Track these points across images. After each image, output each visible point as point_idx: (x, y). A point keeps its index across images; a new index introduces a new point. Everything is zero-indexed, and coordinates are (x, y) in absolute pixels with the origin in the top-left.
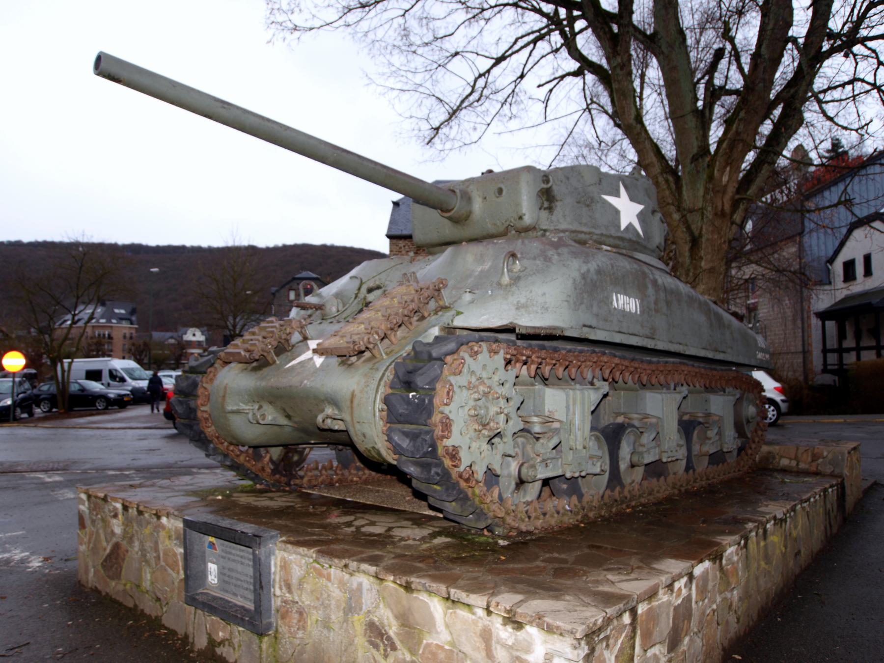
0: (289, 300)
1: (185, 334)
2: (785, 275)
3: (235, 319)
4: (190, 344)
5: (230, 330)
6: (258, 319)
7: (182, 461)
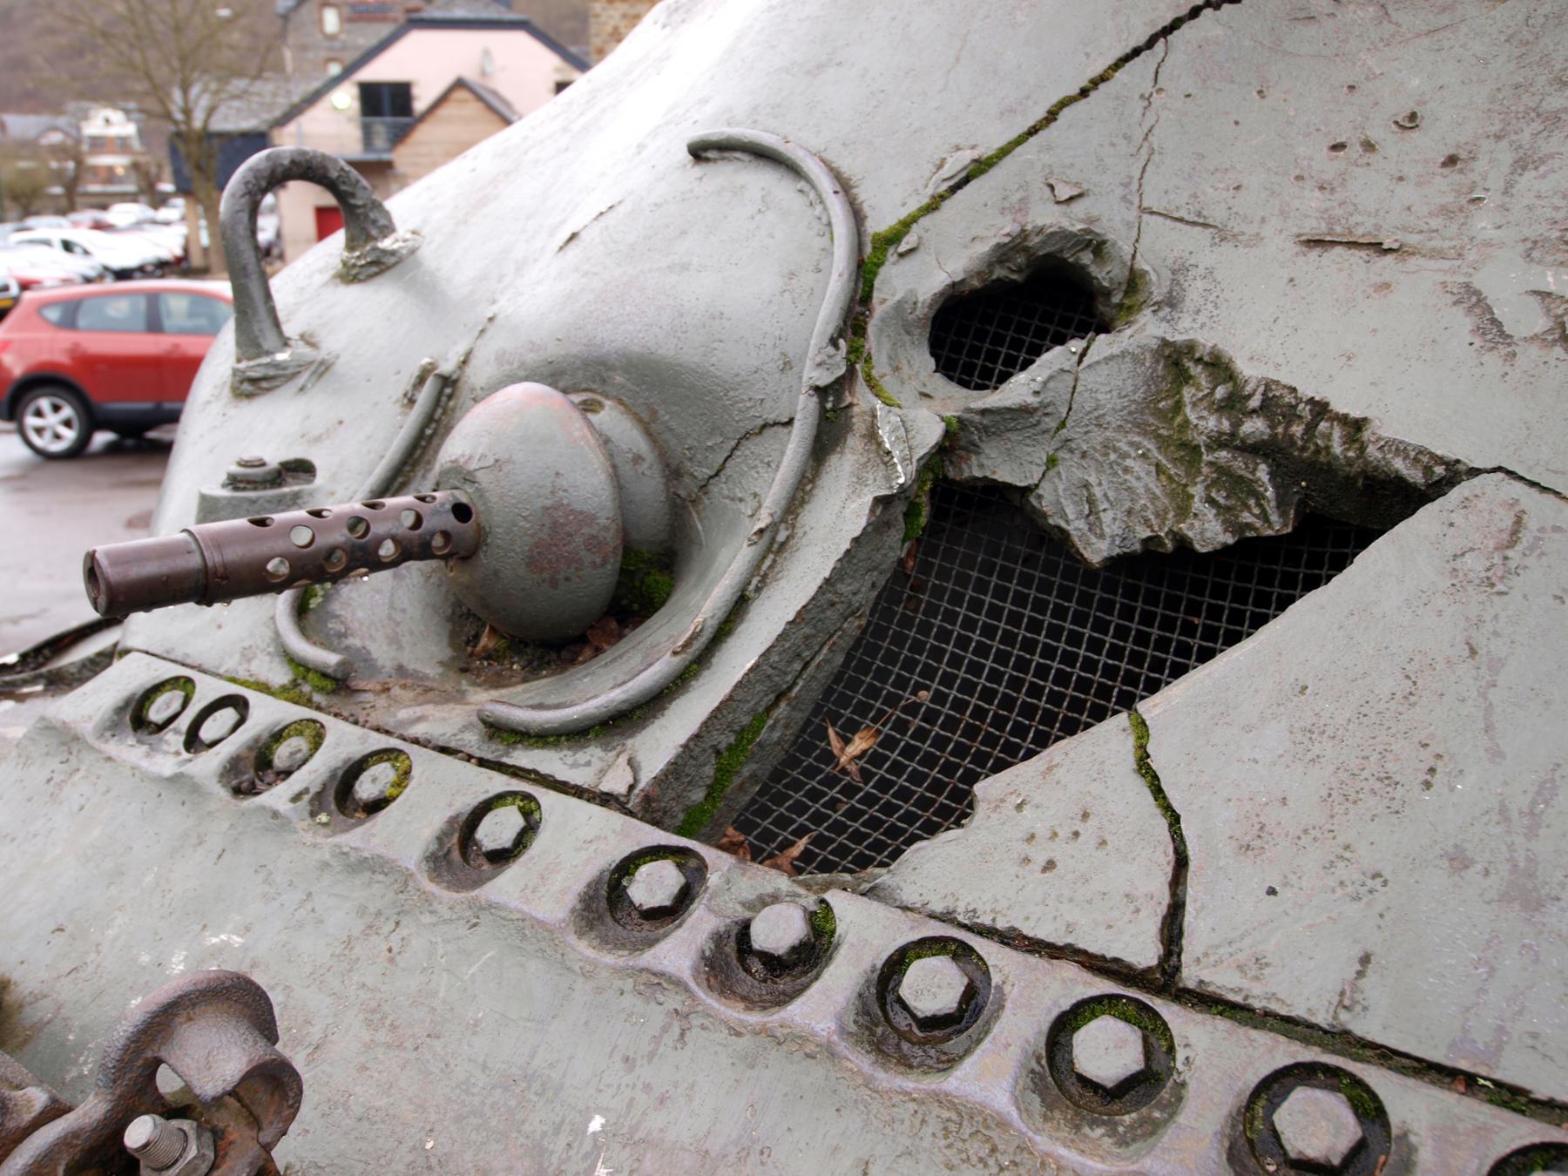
0: (322, 31)
1: (86, 118)
2: (817, 1045)
3: (185, 89)
4: (99, 144)
5: (176, 122)
6: (245, 92)
7: (15, 621)
